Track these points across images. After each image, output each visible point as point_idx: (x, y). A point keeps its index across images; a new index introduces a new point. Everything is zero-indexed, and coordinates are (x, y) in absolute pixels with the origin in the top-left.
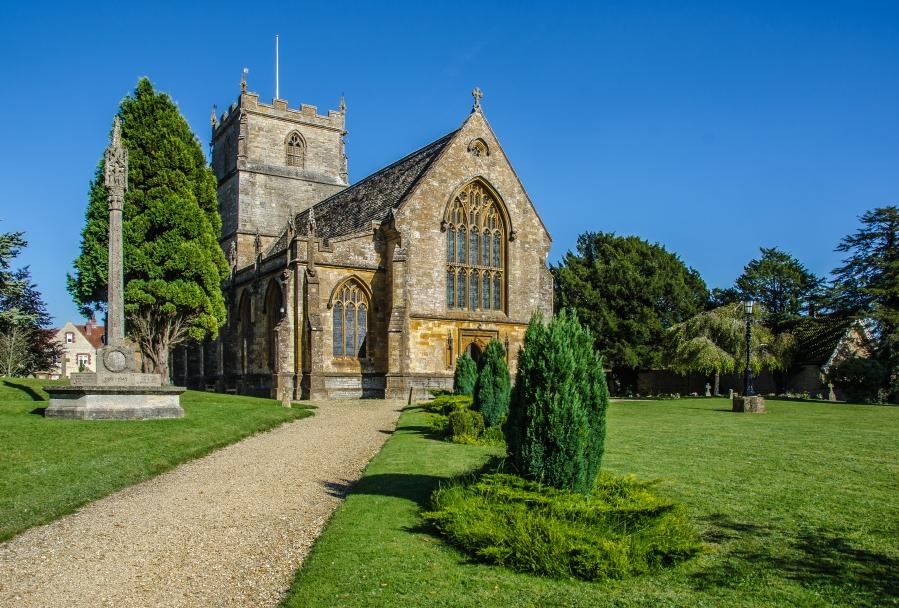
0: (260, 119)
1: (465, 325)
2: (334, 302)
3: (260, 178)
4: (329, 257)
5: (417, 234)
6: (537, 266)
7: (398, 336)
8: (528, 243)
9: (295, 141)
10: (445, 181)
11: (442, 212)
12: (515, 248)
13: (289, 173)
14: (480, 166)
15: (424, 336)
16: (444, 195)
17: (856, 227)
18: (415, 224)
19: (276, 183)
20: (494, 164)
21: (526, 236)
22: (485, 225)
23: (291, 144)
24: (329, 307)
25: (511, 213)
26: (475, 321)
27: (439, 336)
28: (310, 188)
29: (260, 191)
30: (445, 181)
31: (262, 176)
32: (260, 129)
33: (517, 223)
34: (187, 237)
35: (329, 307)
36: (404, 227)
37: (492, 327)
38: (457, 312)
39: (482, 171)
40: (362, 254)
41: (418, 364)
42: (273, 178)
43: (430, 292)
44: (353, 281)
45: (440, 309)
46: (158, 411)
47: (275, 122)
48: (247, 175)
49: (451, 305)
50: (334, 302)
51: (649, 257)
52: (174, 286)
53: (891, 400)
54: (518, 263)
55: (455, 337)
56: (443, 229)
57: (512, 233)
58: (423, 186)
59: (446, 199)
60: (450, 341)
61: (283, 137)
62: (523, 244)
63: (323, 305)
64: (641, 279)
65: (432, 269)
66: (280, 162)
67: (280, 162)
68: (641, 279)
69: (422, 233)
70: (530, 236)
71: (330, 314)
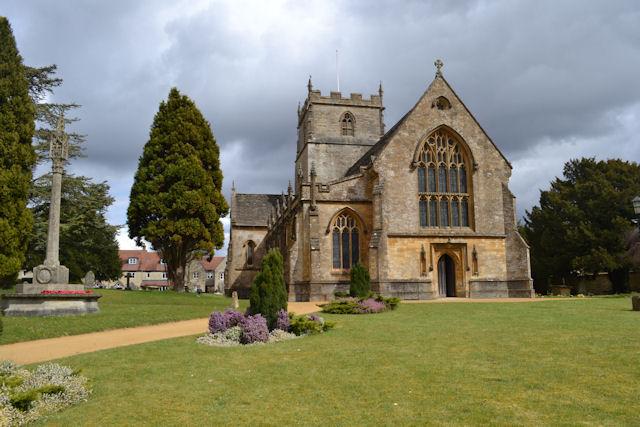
0: (323, 107)
1: (437, 241)
2: (332, 228)
3: (323, 147)
4: (327, 196)
5: (392, 173)
6: (500, 189)
7: (375, 251)
8: (491, 171)
9: (348, 118)
11: (412, 154)
12: (478, 179)
13: (343, 140)
15: (401, 250)
16: (413, 142)
18: (391, 165)
20: (456, 114)
21: (488, 166)
22: (440, 160)
23: (344, 121)
26: (444, 237)
27: (414, 249)
28: (359, 150)
29: (323, 155)
30: (414, 132)
32: (322, 113)
33: (478, 157)
34: (192, 186)
35: (328, 232)
36: (381, 168)
37: (463, 241)
38: (430, 230)
41: (395, 272)
43: (405, 216)
44: (345, 212)
46: (58, 311)
47: (333, 107)
49: (424, 223)
52: (180, 224)
53: (618, 284)
54: (482, 188)
55: (427, 250)
56: (413, 167)
57: (475, 165)
58: (396, 137)
59: (416, 144)
61: (338, 117)
62: (485, 173)
64: (616, 192)
65: (406, 198)
67: (336, 134)
68: (616, 192)
69: (396, 172)
70: (492, 166)
71: (329, 237)
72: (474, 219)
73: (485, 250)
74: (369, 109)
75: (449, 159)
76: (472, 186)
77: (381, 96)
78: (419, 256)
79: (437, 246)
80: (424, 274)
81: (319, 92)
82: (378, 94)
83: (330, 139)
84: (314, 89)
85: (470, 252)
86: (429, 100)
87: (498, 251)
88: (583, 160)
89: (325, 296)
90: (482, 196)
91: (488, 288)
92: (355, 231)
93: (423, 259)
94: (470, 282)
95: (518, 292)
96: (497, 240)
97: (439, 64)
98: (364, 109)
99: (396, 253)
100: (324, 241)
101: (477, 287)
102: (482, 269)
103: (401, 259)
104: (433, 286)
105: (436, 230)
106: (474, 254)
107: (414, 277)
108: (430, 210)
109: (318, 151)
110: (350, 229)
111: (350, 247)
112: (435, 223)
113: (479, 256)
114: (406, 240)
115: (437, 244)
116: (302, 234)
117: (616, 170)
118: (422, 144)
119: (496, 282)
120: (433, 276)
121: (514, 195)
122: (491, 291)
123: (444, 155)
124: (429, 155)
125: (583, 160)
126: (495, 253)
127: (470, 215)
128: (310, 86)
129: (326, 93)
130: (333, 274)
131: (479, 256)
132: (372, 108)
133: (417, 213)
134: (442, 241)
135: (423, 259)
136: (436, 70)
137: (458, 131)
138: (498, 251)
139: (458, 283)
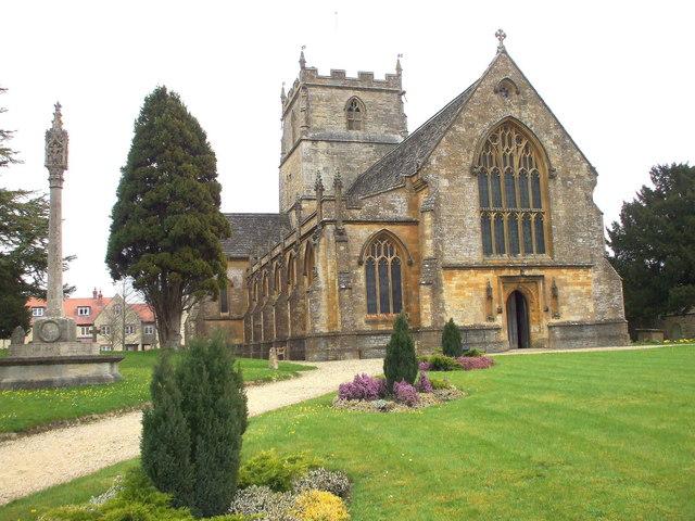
0: (319, 90)
1: (505, 273)
3: (322, 146)
4: (357, 214)
5: (445, 183)
7: (428, 289)
9: (353, 107)
10: (472, 126)
14: (510, 106)
15: (460, 287)
16: (472, 140)
17: (427, 398)
18: (443, 172)
19: (336, 148)
20: (525, 102)
23: (350, 110)
24: (360, 263)
25: (549, 150)
26: (515, 268)
29: (322, 157)
30: (472, 126)
31: (324, 143)
35: (360, 263)
38: (495, 259)
39: (513, 112)
40: (392, 208)
42: (335, 144)
45: (476, 256)
47: (334, 91)
48: (309, 144)
49: (487, 251)
50: (365, 258)
51: (175, 99)
57: (551, 170)
60: (489, 290)
61: (342, 104)
62: (564, 181)
63: (354, 262)
66: (340, 128)
67: (340, 128)
71: (361, 271)
72: (551, 244)
74: (384, 94)
75: (516, 163)
76: (548, 199)
78: (483, 294)
79: (507, 280)
80: (491, 318)
81: (314, 70)
82: (395, 72)
84: (308, 65)
85: (548, 286)
87: (581, 284)
89: (360, 352)
91: (572, 334)
92: (395, 262)
93: (489, 298)
94: (550, 327)
95: (611, 337)
96: (582, 271)
97: (501, 35)
99: (454, 291)
100: (355, 277)
101: (558, 333)
102: (564, 309)
103: (461, 298)
104: (502, 334)
105: (505, 258)
106: (554, 289)
108: (496, 234)
109: (316, 151)
110: (390, 259)
112: (501, 251)
114: (466, 273)
116: (325, 268)
118: (484, 142)
119: (581, 326)
120: (500, 320)
121: (602, 210)
122: (577, 338)
123: (511, 157)
124: (491, 156)
125: (674, 165)
126: (579, 288)
127: (546, 238)
128: (302, 62)
129: (324, 72)
131: (561, 292)
132: (388, 91)
133: (479, 236)
134: (512, 273)
135: (489, 298)
137: (529, 125)
139: (534, 328)
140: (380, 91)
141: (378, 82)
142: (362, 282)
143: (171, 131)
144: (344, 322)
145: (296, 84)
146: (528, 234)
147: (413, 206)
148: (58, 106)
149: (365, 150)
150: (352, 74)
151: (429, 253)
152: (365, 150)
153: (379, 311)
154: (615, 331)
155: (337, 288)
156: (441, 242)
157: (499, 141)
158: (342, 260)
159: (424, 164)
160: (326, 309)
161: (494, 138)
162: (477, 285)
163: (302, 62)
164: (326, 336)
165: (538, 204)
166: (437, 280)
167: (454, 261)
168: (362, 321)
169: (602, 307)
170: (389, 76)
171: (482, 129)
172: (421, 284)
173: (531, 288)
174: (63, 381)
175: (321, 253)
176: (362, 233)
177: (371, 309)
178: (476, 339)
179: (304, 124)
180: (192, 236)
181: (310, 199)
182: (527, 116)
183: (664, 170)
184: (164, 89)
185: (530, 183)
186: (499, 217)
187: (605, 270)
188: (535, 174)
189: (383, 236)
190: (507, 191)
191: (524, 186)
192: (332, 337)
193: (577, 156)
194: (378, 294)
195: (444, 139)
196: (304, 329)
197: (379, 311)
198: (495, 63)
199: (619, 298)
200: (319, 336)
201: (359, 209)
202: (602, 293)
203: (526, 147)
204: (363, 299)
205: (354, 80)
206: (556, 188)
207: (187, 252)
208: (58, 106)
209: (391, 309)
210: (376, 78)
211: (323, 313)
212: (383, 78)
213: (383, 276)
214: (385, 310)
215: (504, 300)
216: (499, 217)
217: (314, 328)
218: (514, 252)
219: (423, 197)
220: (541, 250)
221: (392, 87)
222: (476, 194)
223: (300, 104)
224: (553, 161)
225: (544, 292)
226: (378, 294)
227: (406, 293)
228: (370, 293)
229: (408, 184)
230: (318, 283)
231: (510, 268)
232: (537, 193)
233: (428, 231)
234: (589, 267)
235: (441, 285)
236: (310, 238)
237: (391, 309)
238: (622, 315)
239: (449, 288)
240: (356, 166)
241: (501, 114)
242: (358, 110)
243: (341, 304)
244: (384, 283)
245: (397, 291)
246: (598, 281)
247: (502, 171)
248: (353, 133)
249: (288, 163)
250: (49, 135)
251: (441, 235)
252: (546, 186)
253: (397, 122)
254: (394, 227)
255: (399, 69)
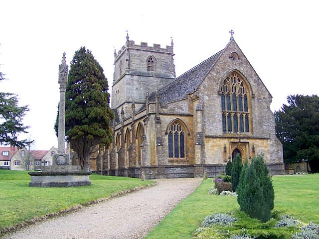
1: (232, 140)
3: (136, 77)
4: (165, 111)
5: (206, 98)
7: (199, 146)
8: (261, 99)
9: (150, 60)
10: (219, 72)
16: (219, 79)
18: (206, 93)
19: (142, 79)
20: (242, 63)
23: (149, 61)
24: (166, 134)
25: (252, 85)
26: (237, 138)
28: (159, 80)
29: (135, 83)
30: (219, 72)
35: (166, 134)
38: (228, 134)
40: (181, 108)
42: (141, 77)
43: (214, 125)
47: (142, 52)
49: (224, 130)
50: (168, 131)
51: (89, 53)
54: (256, 109)
60: (225, 148)
61: (146, 58)
62: (258, 99)
63: (164, 133)
71: (167, 137)
73: (259, 147)
74: (165, 55)
75: (237, 91)
77: (172, 46)
78: (223, 150)
81: (133, 42)
83: (140, 73)
85: (251, 147)
86: (226, 54)
87: (265, 147)
88: (313, 95)
90: (257, 114)
93: (225, 151)
95: (277, 171)
96: (265, 141)
97: (232, 32)
98: (162, 55)
99: (210, 148)
103: (213, 151)
106: (253, 148)
107: (220, 163)
109: (133, 80)
110: (179, 132)
111: (179, 144)
113: (256, 150)
114: (215, 140)
115: (233, 142)
116: (150, 135)
117: (76, 146)
124: (226, 87)
126: (264, 148)
128: (128, 38)
129: (137, 43)
130: (169, 161)
132: (167, 54)
136: (230, 36)
137: (243, 73)
138: (265, 147)
140: (164, 53)
141: (137, 46)
142: (166, 143)
143: (89, 68)
144: (159, 161)
145: (123, 47)
146: (242, 122)
147: (191, 108)
148: (64, 54)
149: (156, 81)
150: (150, 45)
151: (200, 130)
152: (156, 81)
153: (174, 157)
154: (278, 168)
155: (156, 145)
156: (204, 125)
157: (230, 80)
158: (158, 132)
159: (197, 89)
160: (150, 155)
161: (228, 79)
162: (220, 145)
163: (128, 38)
164: (150, 168)
165: (246, 110)
166: (203, 143)
167: (210, 134)
168: (166, 161)
169: (274, 157)
170: (168, 47)
171: (223, 75)
172: (196, 144)
173: (243, 148)
174: (72, 183)
175: (148, 128)
176: (167, 120)
177: (171, 155)
178: (219, 170)
179: (127, 67)
180: (99, 118)
181: (129, 103)
182: (243, 69)
183: (293, 97)
184: (84, 48)
185: (243, 100)
186: (229, 115)
187: (275, 141)
188: (245, 96)
189: (176, 121)
190: (233, 103)
191: (240, 101)
192: (153, 168)
193: (264, 89)
194: (174, 148)
195: (206, 78)
196: (135, 164)
197: (174, 157)
198: (229, 45)
199: (281, 153)
200: (146, 167)
201: (166, 108)
202: (274, 151)
203: (242, 84)
204: (167, 151)
205: (152, 48)
206: (255, 103)
207: (96, 125)
208: (64, 54)
209: (180, 156)
210: (161, 47)
211: (148, 157)
212: (165, 48)
213: (176, 140)
214: (177, 156)
215: (231, 153)
216: (229, 115)
217: (144, 164)
218: (242, 131)
219: (196, 104)
220: (248, 131)
221: (169, 52)
222: (221, 104)
223: (125, 57)
224: (254, 90)
225: (249, 150)
226: (174, 148)
227: (187, 149)
228: (170, 148)
229: (189, 98)
230: (147, 142)
231: (234, 138)
232: (246, 104)
233: (199, 120)
234: (268, 139)
235: (204, 145)
236: (142, 121)
237: (180, 156)
238: (282, 162)
239: (208, 147)
240: (151, 88)
241: (232, 68)
242: (152, 62)
243: (158, 152)
244: (176, 144)
245: (182, 148)
246: (272, 145)
247: (231, 93)
248: (150, 72)
249: (116, 85)
250: (60, 66)
251: (205, 122)
252: (251, 102)
253: (170, 68)
254: (182, 117)
255: (172, 44)
